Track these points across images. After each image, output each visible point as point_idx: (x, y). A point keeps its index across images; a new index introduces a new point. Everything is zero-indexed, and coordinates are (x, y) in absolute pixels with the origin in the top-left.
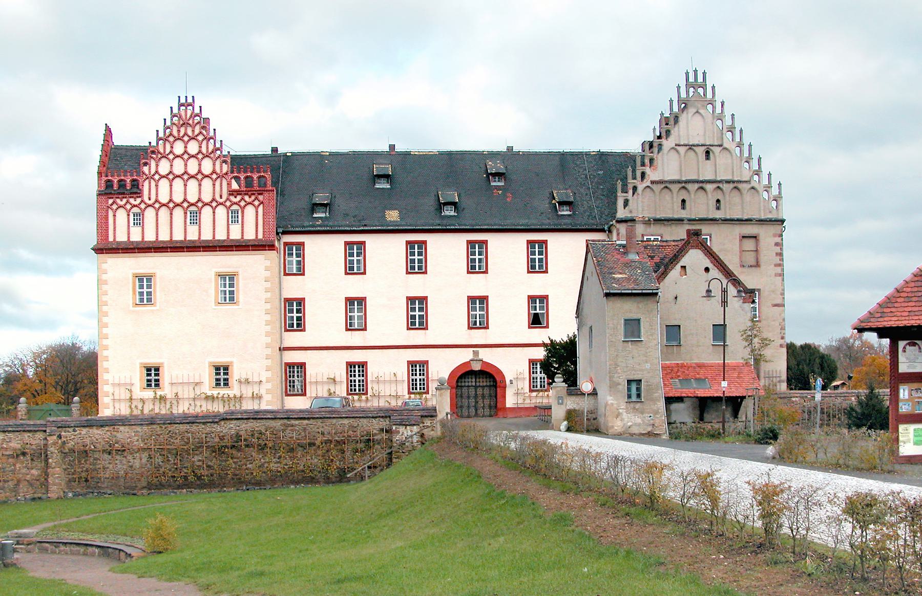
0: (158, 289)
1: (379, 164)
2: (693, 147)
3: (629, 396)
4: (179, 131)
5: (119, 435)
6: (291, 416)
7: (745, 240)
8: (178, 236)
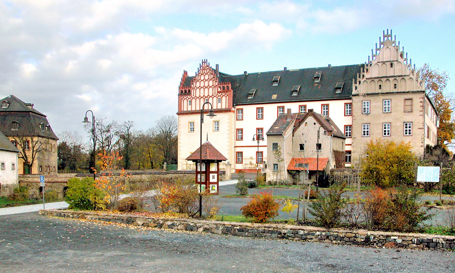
0: (195, 127)
4: (202, 72)
5: (142, 177)
7: (406, 101)
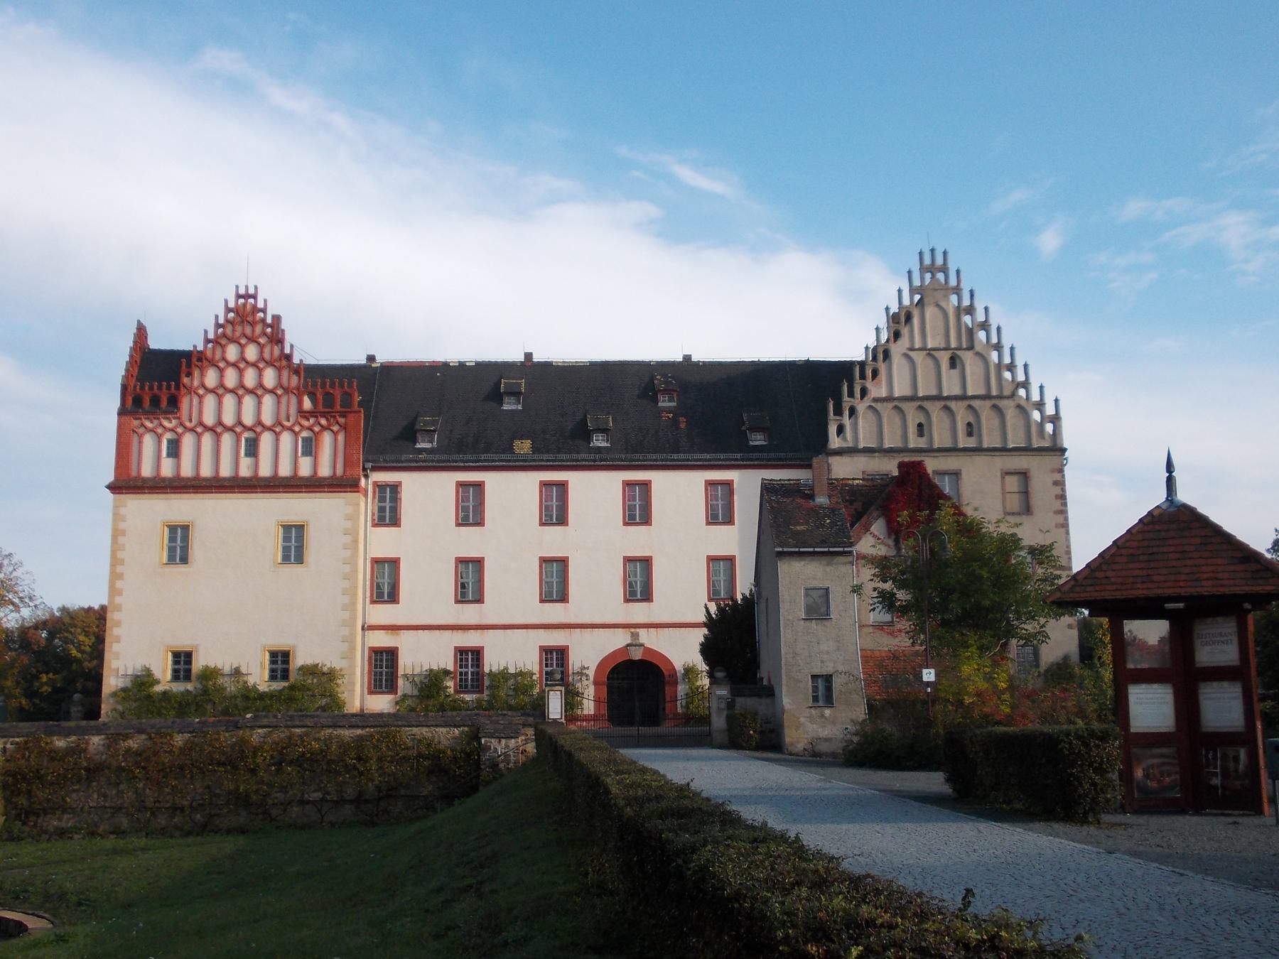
2: (932, 352)
3: (815, 699)
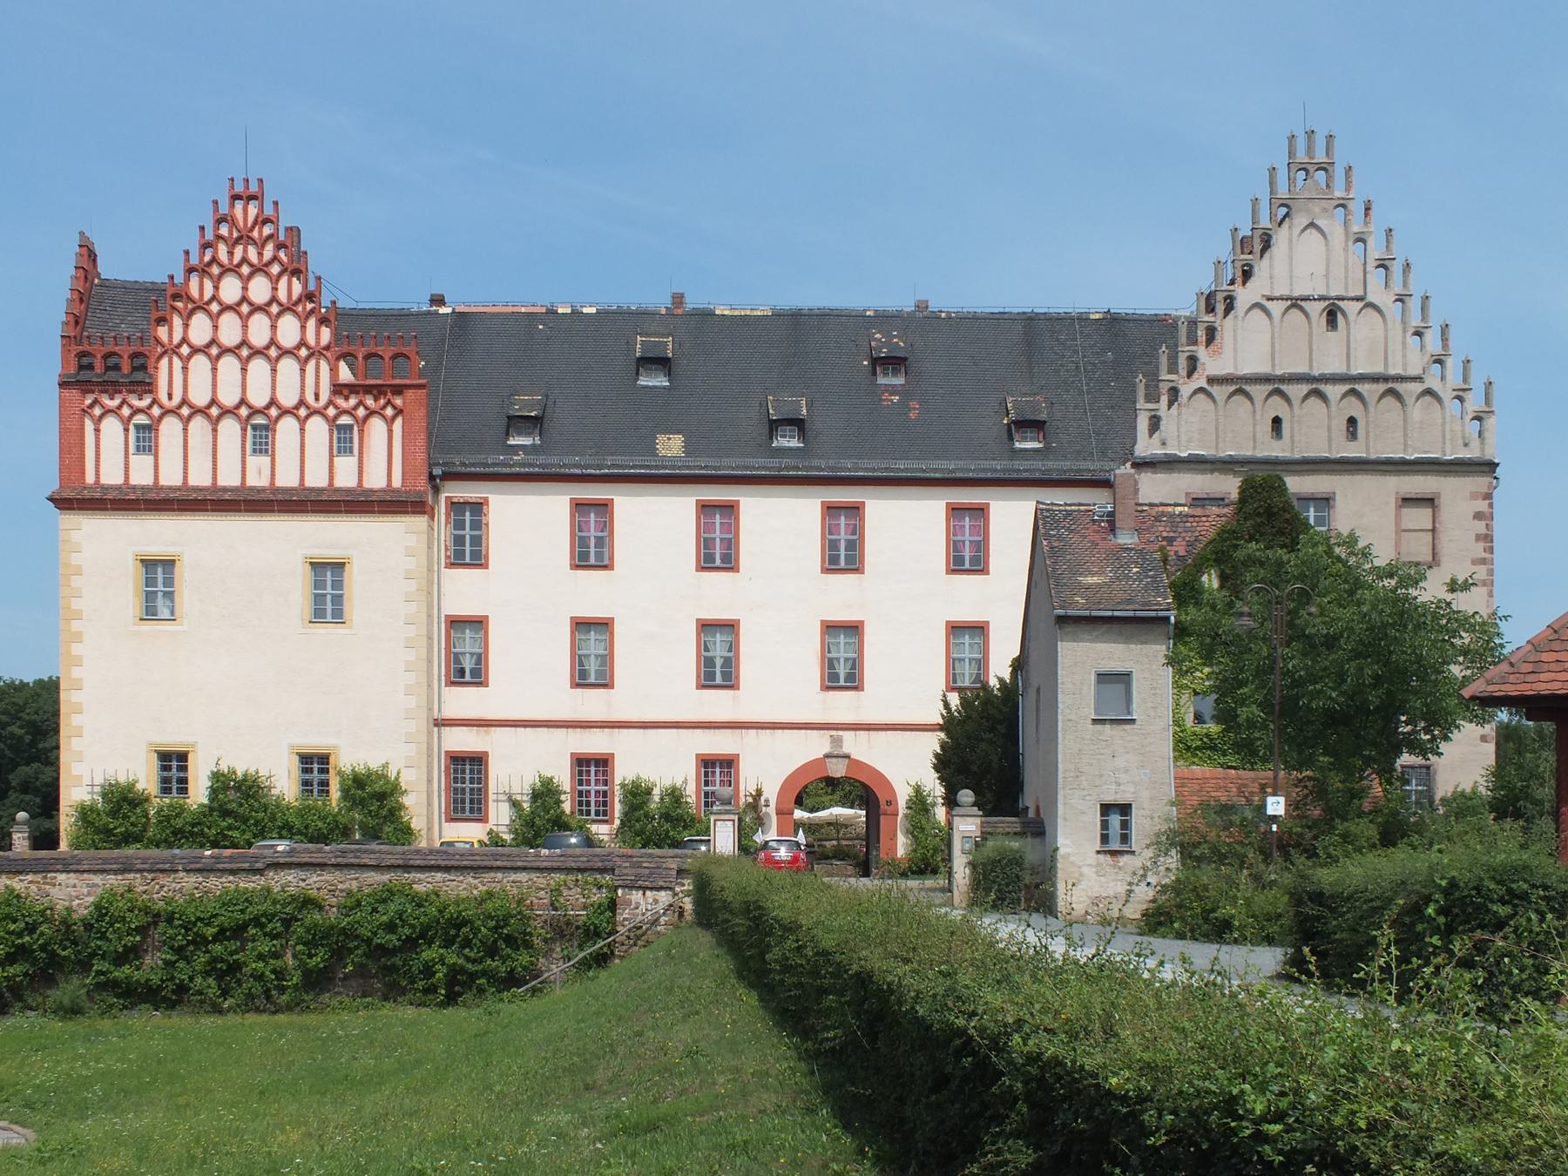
1: (648, 335)
3: (1105, 839)
4: (231, 253)
6: (411, 862)
8: (229, 478)
